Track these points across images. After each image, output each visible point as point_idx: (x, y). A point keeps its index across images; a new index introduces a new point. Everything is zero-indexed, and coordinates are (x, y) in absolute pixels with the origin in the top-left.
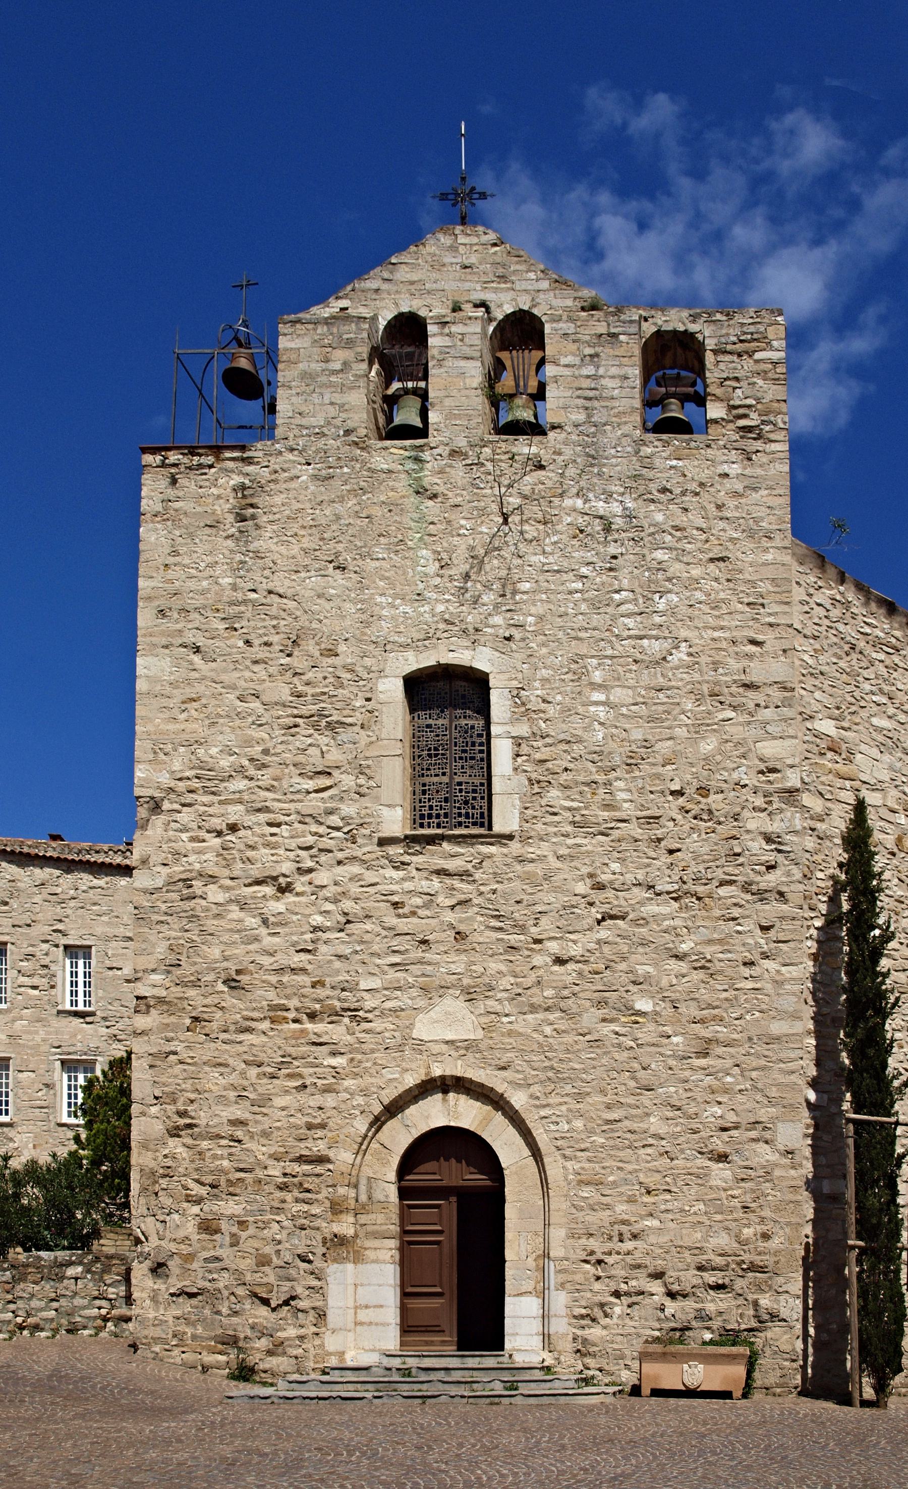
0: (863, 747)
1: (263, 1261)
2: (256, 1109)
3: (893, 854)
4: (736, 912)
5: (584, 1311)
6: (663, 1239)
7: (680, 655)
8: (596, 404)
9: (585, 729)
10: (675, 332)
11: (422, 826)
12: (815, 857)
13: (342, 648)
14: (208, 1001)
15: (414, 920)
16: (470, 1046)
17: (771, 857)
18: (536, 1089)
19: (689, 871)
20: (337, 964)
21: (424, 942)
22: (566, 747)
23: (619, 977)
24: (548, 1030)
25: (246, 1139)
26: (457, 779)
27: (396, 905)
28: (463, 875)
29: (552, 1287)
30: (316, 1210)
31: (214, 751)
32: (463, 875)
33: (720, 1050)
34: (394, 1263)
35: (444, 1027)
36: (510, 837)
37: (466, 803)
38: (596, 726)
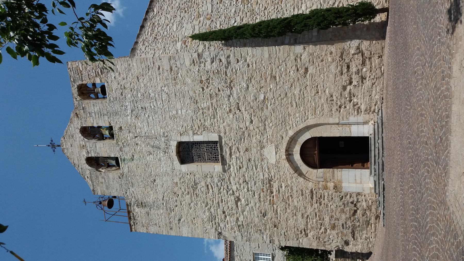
0: (183, 33)
1: (343, 211)
2: (298, 210)
3: (212, 21)
4: (234, 70)
5: (356, 111)
6: (333, 87)
7: (166, 89)
8: (102, 113)
9: (189, 115)
10: (78, 91)
11: (218, 160)
12: (216, 47)
13: (175, 181)
14: (270, 223)
15: (244, 163)
16: (277, 147)
17: (218, 61)
18: (288, 128)
19: (224, 85)
20: (257, 185)
21: (249, 160)
22: (194, 121)
23: (254, 104)
24: (271, 125)
25: (307, 214)
26: (205, 150)
27: (240, 168)
28: (230, 149)
29: (348, 122)
30: (326, 194)
31: (205, 217)
32: (230, 149)
33: (274, 73)
34: (342, 171)
35: (273, 155)
36: (220, 136)
37: (211, 148)
38: (188, 112)
